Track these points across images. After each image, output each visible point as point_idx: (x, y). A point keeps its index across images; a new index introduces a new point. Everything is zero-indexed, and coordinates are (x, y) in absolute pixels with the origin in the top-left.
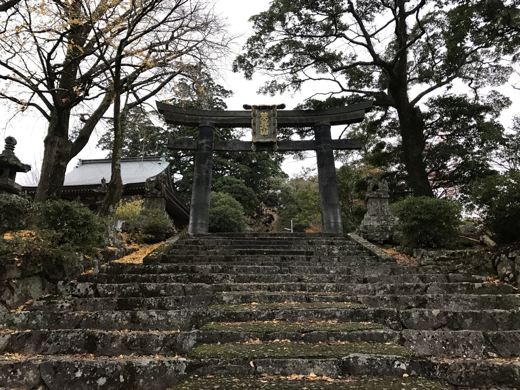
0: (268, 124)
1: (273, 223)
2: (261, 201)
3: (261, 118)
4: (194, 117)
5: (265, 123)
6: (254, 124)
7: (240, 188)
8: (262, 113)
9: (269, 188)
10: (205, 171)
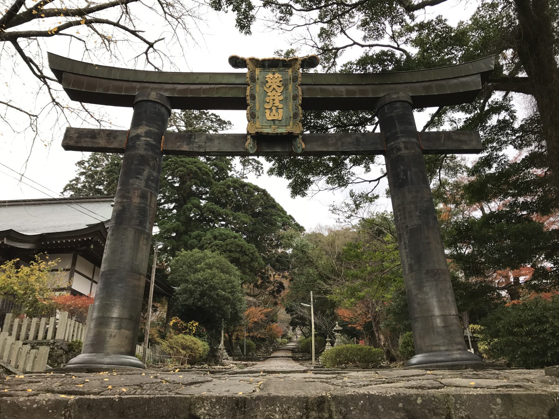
0: (281, 98)
1: (283, 294)
2: (267, 264)
3: (268, 85)
4: (125, 84)
5: (276, 96)
6: (253, 97)
7: (238, 245)
8: (270, 75)
9: (277, 246)
10: (137, 193)
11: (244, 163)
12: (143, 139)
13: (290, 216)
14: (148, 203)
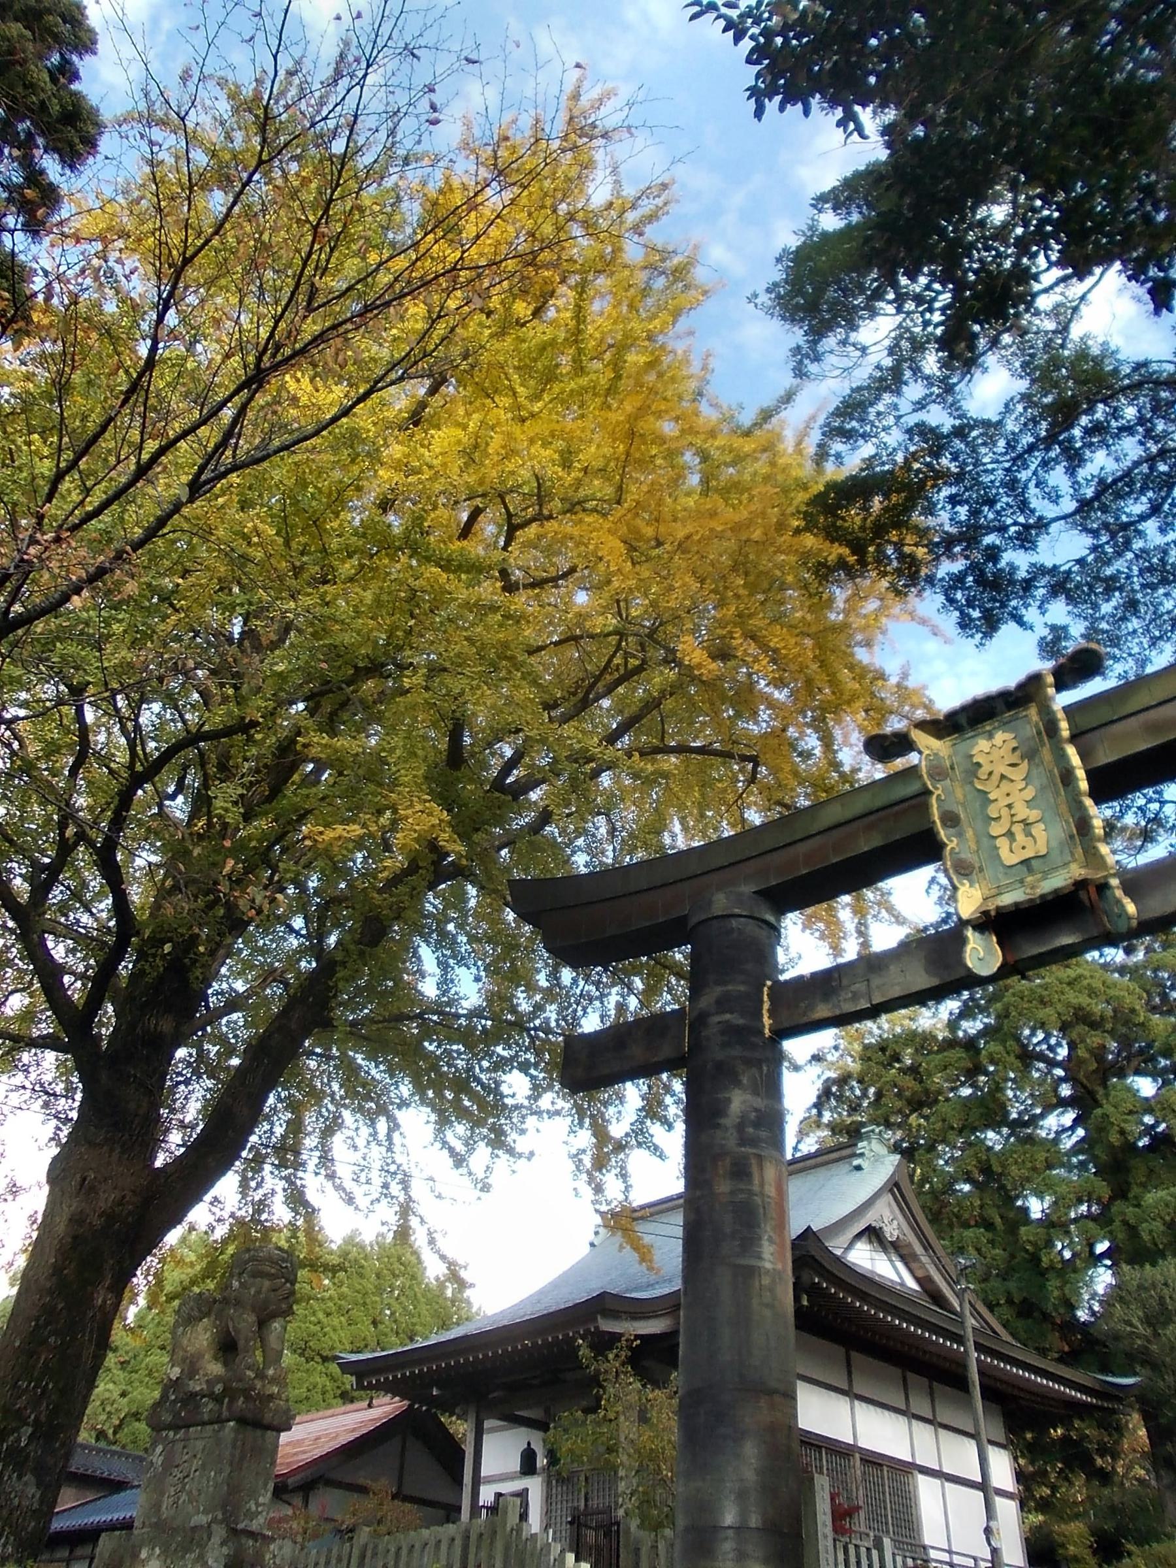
0: (1030, 793)
3: (982, 773)
8: (983, 744)
12: (716, 1019)
14: (756, 1188)
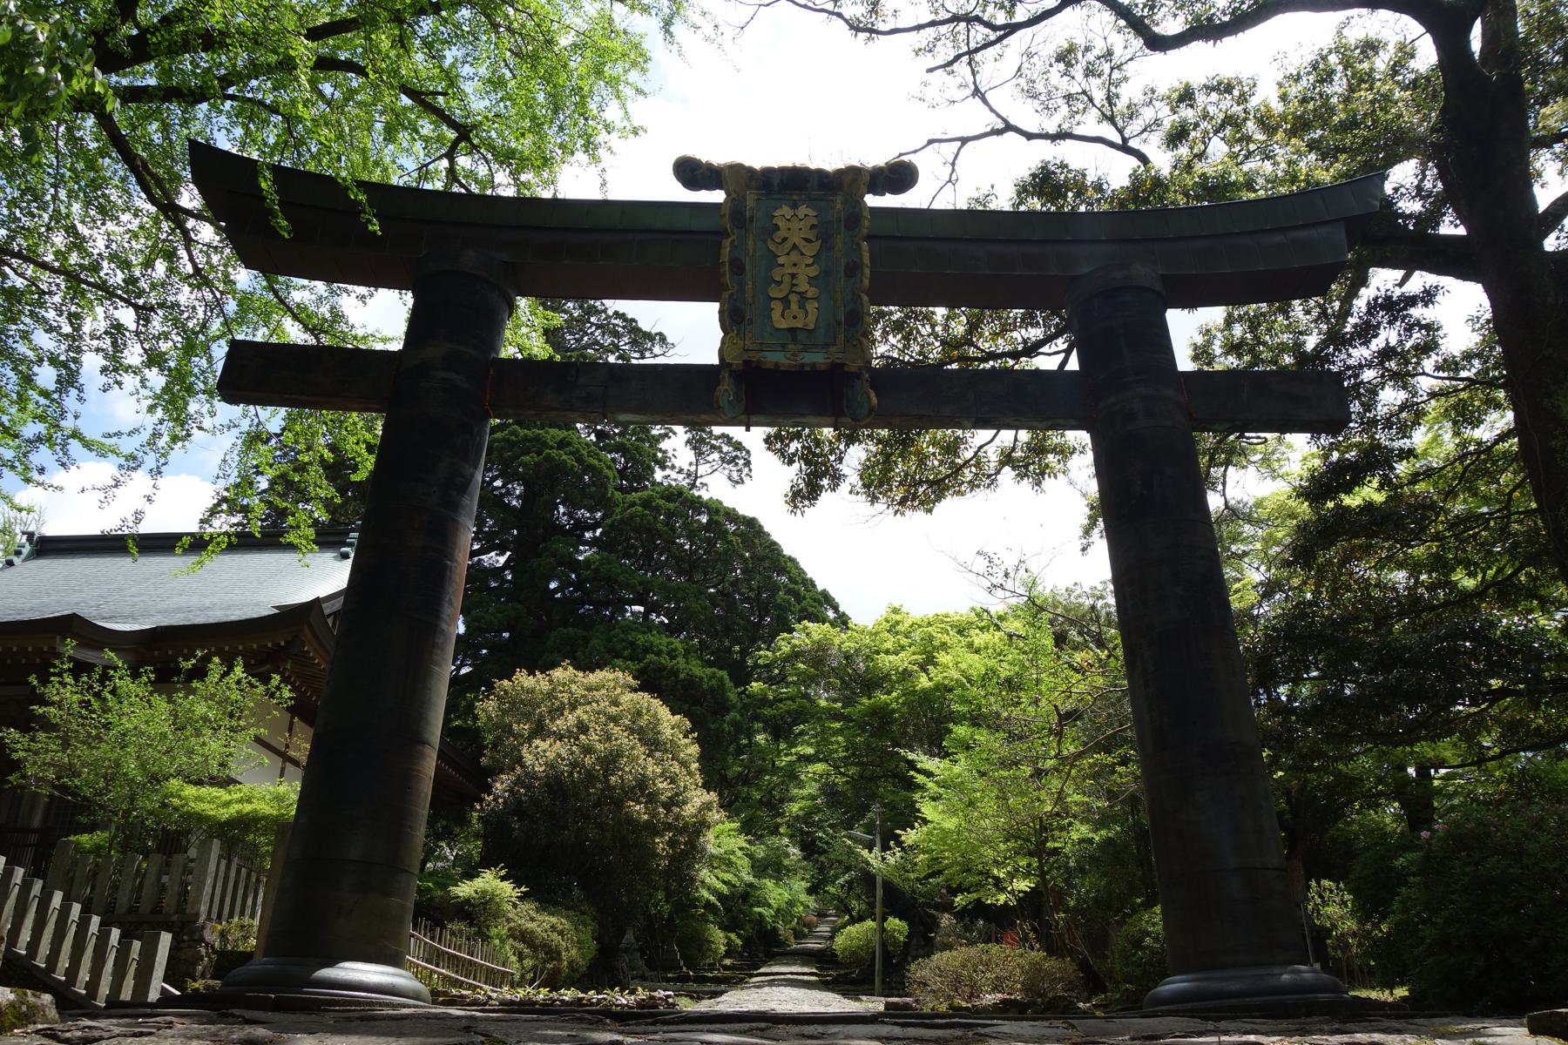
0: (814, 271)
3: (778, 236)
6: (738, 267)
11: (697, 445)
13: (825, 594)
